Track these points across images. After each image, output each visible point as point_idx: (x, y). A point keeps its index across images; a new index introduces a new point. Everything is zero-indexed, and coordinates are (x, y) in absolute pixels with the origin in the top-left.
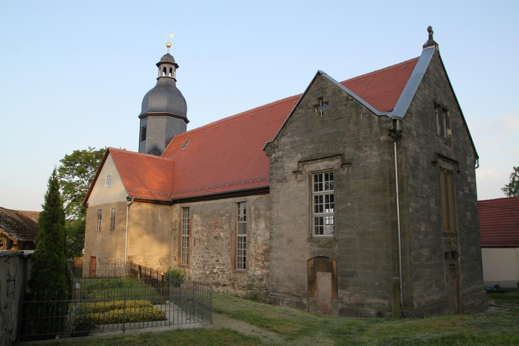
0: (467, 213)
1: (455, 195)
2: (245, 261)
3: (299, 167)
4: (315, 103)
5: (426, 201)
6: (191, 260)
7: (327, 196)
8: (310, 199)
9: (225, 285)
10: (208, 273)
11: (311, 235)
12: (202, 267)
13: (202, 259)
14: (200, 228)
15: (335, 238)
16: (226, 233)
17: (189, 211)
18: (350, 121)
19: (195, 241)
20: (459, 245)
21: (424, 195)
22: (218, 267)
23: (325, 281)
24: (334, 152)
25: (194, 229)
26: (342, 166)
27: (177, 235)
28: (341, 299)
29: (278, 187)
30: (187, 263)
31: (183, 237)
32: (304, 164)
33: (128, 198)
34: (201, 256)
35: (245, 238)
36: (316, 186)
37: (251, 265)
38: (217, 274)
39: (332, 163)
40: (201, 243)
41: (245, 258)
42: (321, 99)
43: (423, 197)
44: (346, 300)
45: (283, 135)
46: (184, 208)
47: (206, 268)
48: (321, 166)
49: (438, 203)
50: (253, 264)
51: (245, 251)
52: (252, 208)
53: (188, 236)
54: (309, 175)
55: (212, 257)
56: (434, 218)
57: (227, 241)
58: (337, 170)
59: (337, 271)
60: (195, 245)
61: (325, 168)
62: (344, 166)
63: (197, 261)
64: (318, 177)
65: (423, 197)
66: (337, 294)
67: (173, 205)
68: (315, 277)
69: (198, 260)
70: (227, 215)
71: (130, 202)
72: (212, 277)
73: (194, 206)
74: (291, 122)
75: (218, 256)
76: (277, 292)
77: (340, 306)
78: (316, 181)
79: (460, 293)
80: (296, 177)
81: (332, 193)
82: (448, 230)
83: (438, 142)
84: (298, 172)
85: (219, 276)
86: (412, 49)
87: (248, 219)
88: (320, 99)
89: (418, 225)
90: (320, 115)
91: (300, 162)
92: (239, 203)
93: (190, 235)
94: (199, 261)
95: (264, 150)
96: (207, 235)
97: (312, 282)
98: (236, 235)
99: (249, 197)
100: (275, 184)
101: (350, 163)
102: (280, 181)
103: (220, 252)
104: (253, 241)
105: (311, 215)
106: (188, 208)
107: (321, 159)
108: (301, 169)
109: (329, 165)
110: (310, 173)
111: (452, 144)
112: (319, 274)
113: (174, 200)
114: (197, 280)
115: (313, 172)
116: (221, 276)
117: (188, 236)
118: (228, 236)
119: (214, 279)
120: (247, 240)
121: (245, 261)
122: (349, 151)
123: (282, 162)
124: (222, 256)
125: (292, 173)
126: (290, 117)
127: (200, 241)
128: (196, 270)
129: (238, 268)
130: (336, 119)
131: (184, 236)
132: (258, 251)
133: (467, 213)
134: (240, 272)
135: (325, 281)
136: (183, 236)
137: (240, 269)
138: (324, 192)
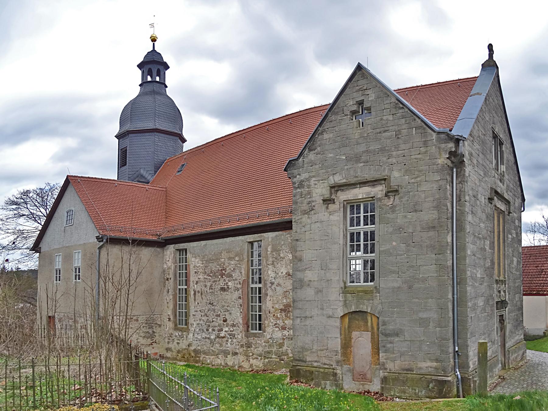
0: (514, 259)
1: (506, 238)
2: (260, 320)
3: (331, 194)
4: (355, 108)
5: (482, 242)
6: (191, 320)
7: (366, 234)
8: (345, 236)
9: (236, 354)
10: (213, 337)
11: (345, 283)
12: (205, 330)
13: (205, 318)
14: (201, 277)
15: (376, 287)
16: (236, 282)
17: (186, 255)
18: (400, 136)
19: (195, 294)
20: (507, 294)
21: (481, 236)
22: (227, 329)
23: (362, 342)
24: (377, 176)
25: (193, 278)
26: (386, 195)
27: (172, 286)
28: (384, 364)
29: (304, 219)
30: (186, 325)
31: (180, 289)
32: (337, 191)
33: (97, 238)
34: (203, 314)
35: (260, 288)
36: (352, 219)
37: (269, 326)
38: (226, 339)
39: (374, 190)
40: (204, 297)
41: (260, 315)
42: (361, 103)
43: (480, 238)
44: (390, 365)
45: (310, 150)
46: (180, 250)
47: (210, 330)
48: (360, 193)
49: (492, 247)
50: (271, 324)
51: (260, 307)
52: (269, 250)
53: (186, 287)
54: (344, 205)
55: (219, 316)
56: (488, 264)
57: (236, 294)
58: (380, 199)
59: (378, 329)
60: (195, 300)
61: (364, 196)
62: (390, 194)
63: (198, 322)
64: (353, 206)
65: (480, 238)
66: (378, 359)
67: (165, 246)
68: (351, 338)
69: (200, 320)
70: (237, 259)
71: (102, 243)
72: (218, 343)
73: (194, 247)
74: (322, 133)
75: (226, 313)
76: (302, 361)
77: (382, 374)
78: (352, 213)
79: (507, 345)
80: (327, 208)
81: (373, 229)
82: (499, 277)
83: (494, 177)
84: (330, 200)
85: (227, 341)
86: (469, 67)
87: (264, 262)
88: (360, 104)
89: (475, 271)
90: (360, 126)
91: (332, 187)
92: (252, 243)
93: (189, 287)
94: (202, 322)
95: (285, 170)
96: (211, 286)
97: (347, 345)
98: (248, 285)
99: (265, 235)
100: (300, 217)
101: (397, 191)
102: (305, 213)
103: (228, 308)
104: (270, 292)
105: (345, 258)
106: (186, 250)
107: (360, 183)
108: (333, 197)
109: (369, 193)
110: (345, 203)
111: (505, 183)
112: (355, 334)
113: (166, 240)
114: (199, 348)
115: (348, 202)
116: (230, 340)
117: (186, 287)
118: (239, 286)
119: (221, 345)
120: (263, 291)
121: (260, 320)
122: (396, 176)
123: (309, 186)
124: (230, 313)
125: (322, 202)
126: (320, 125)
127: (202, 294)
128: (198, 334)
129: (252, 329)
130: (380, 132)
131: (181, 287)
132: (277, 306)
133: (514, 259)
134: (255, 335)
135: (362, 342)
136: (179, 287)
137: (254, 331)
138: (362, 228)
